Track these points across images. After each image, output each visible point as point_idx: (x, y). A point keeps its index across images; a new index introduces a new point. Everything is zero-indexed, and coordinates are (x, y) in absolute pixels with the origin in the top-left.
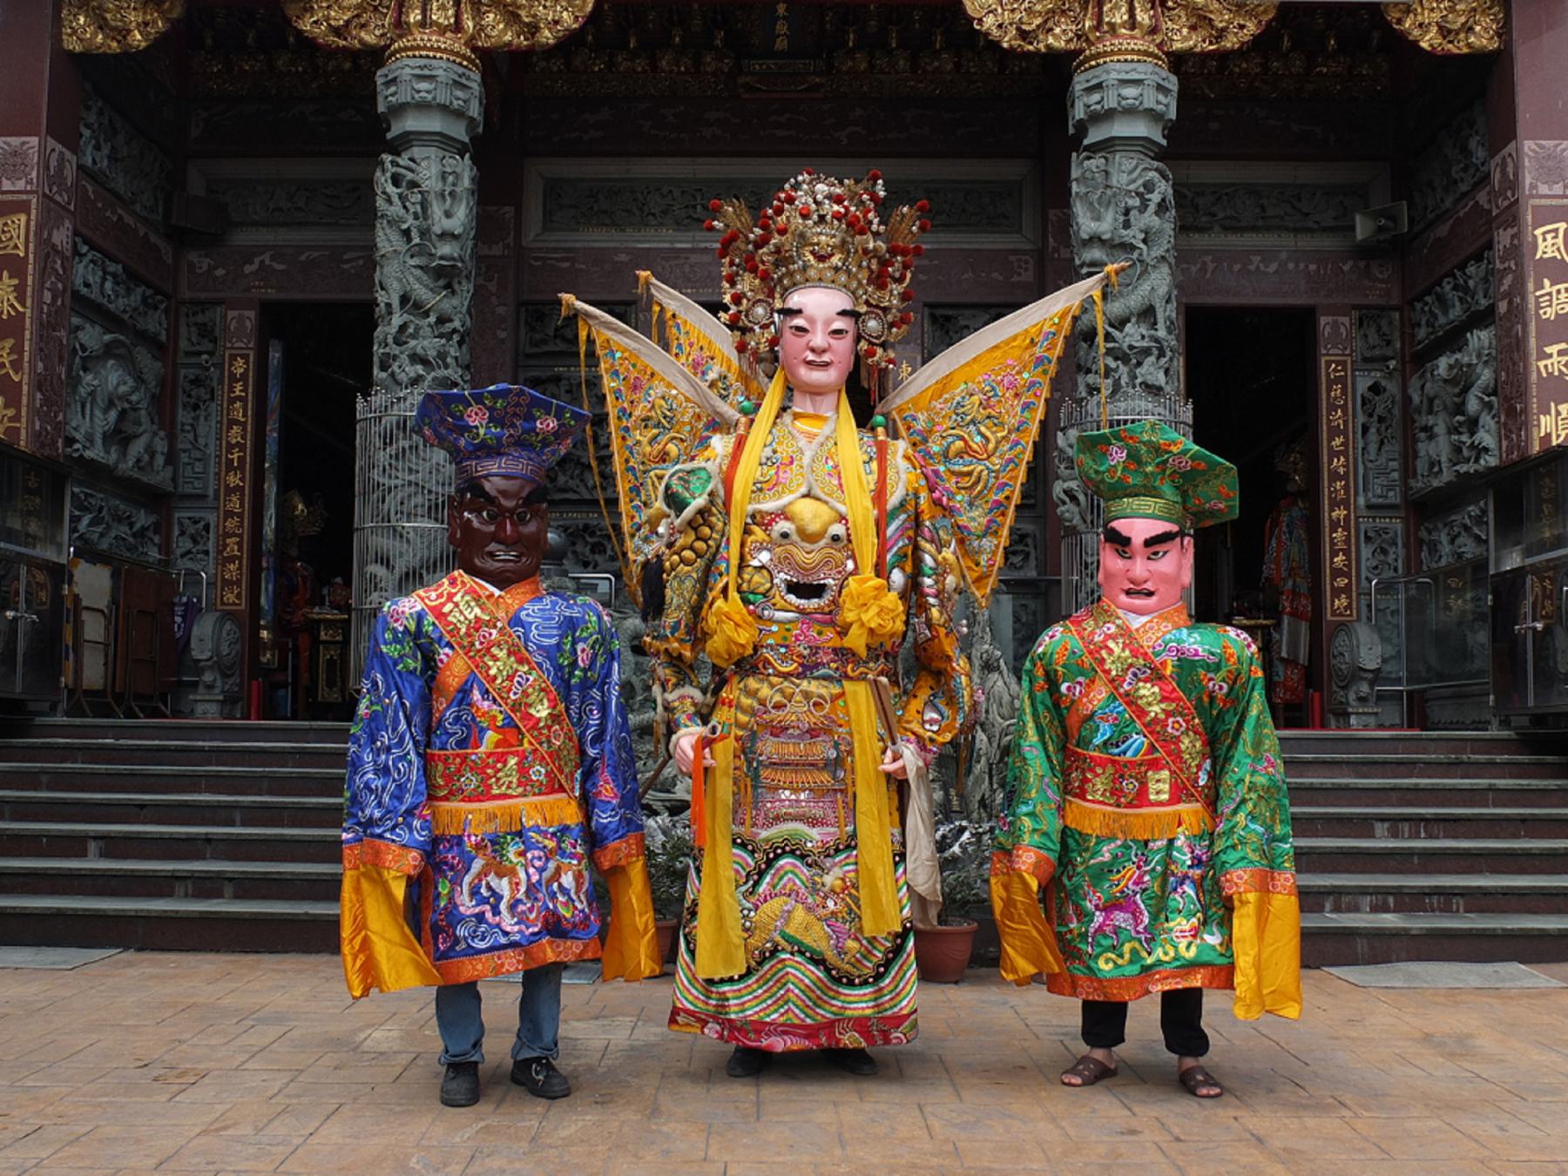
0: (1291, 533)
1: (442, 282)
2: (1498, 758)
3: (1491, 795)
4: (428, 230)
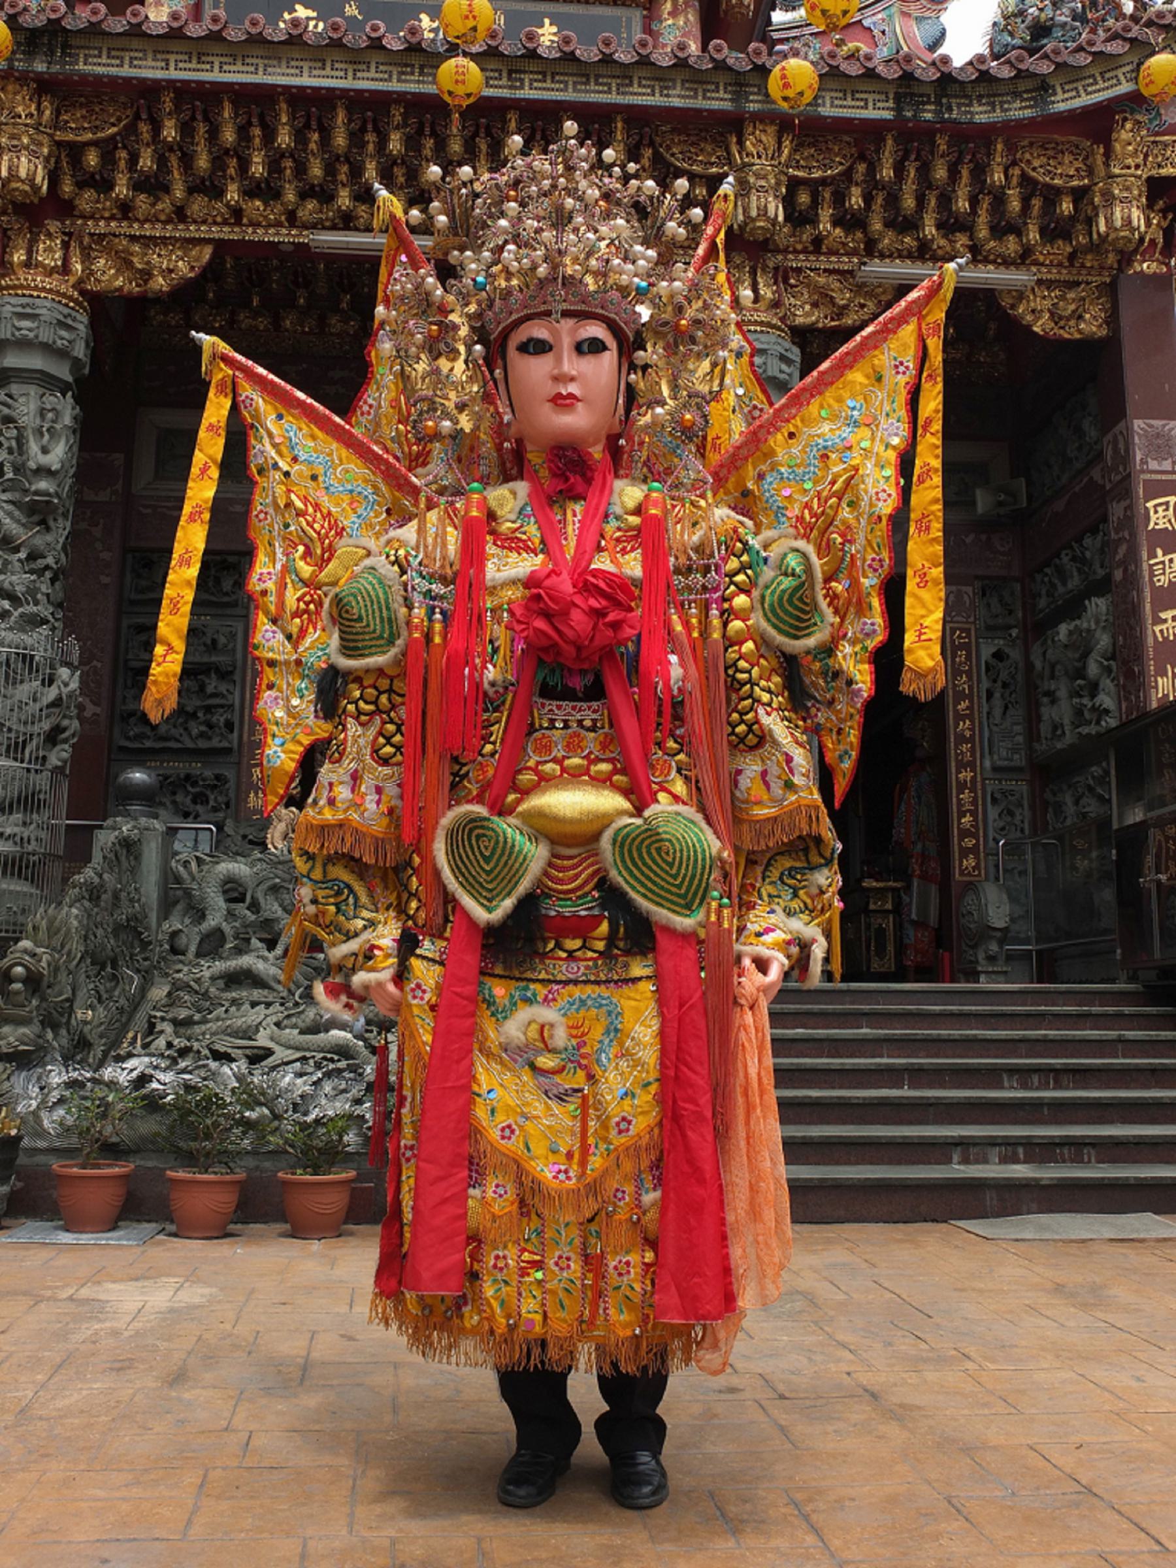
0: (919, 797)
1: (36, 518)
2: (1127, 1010)
3: (1120, 1046)
4: (24, 464)
